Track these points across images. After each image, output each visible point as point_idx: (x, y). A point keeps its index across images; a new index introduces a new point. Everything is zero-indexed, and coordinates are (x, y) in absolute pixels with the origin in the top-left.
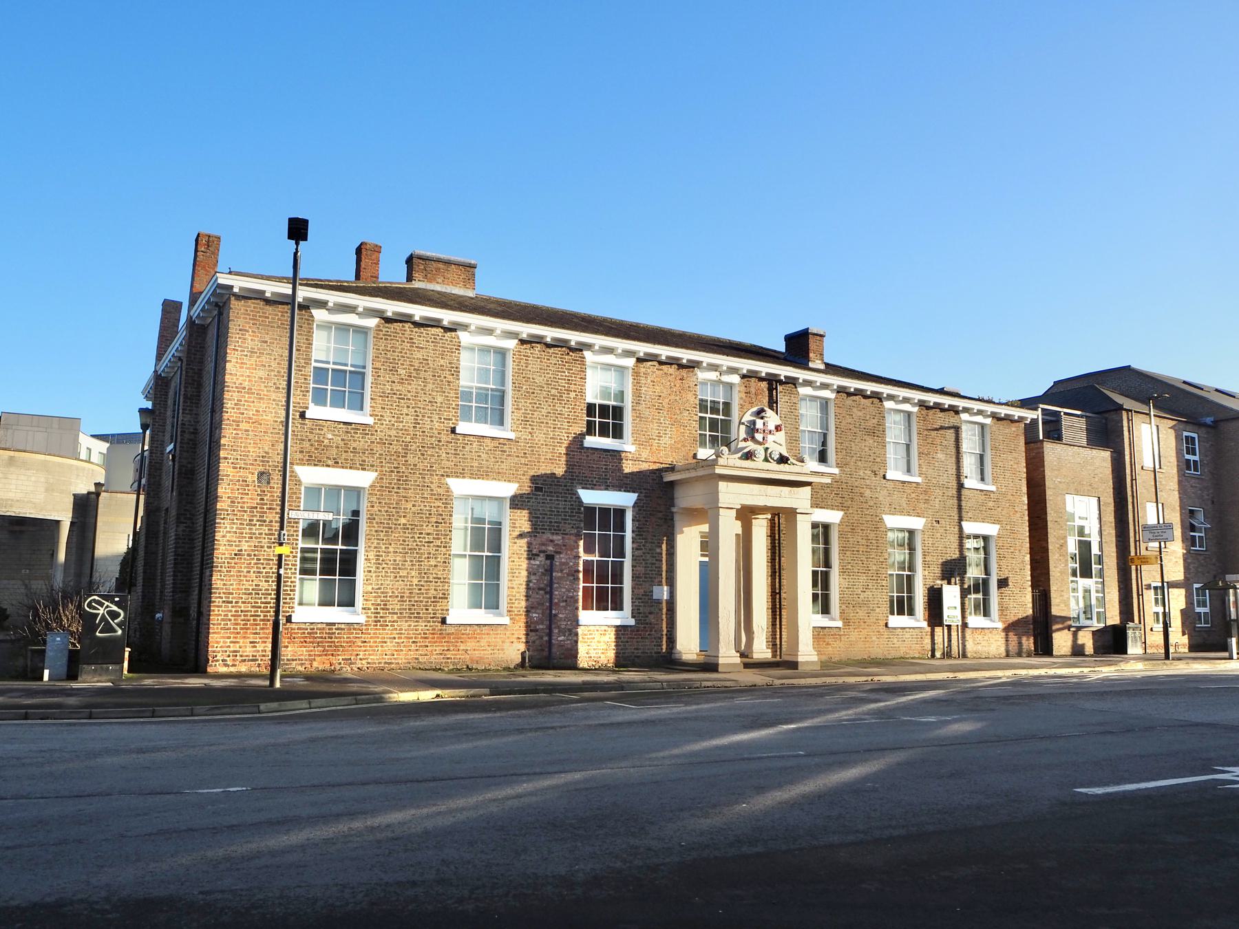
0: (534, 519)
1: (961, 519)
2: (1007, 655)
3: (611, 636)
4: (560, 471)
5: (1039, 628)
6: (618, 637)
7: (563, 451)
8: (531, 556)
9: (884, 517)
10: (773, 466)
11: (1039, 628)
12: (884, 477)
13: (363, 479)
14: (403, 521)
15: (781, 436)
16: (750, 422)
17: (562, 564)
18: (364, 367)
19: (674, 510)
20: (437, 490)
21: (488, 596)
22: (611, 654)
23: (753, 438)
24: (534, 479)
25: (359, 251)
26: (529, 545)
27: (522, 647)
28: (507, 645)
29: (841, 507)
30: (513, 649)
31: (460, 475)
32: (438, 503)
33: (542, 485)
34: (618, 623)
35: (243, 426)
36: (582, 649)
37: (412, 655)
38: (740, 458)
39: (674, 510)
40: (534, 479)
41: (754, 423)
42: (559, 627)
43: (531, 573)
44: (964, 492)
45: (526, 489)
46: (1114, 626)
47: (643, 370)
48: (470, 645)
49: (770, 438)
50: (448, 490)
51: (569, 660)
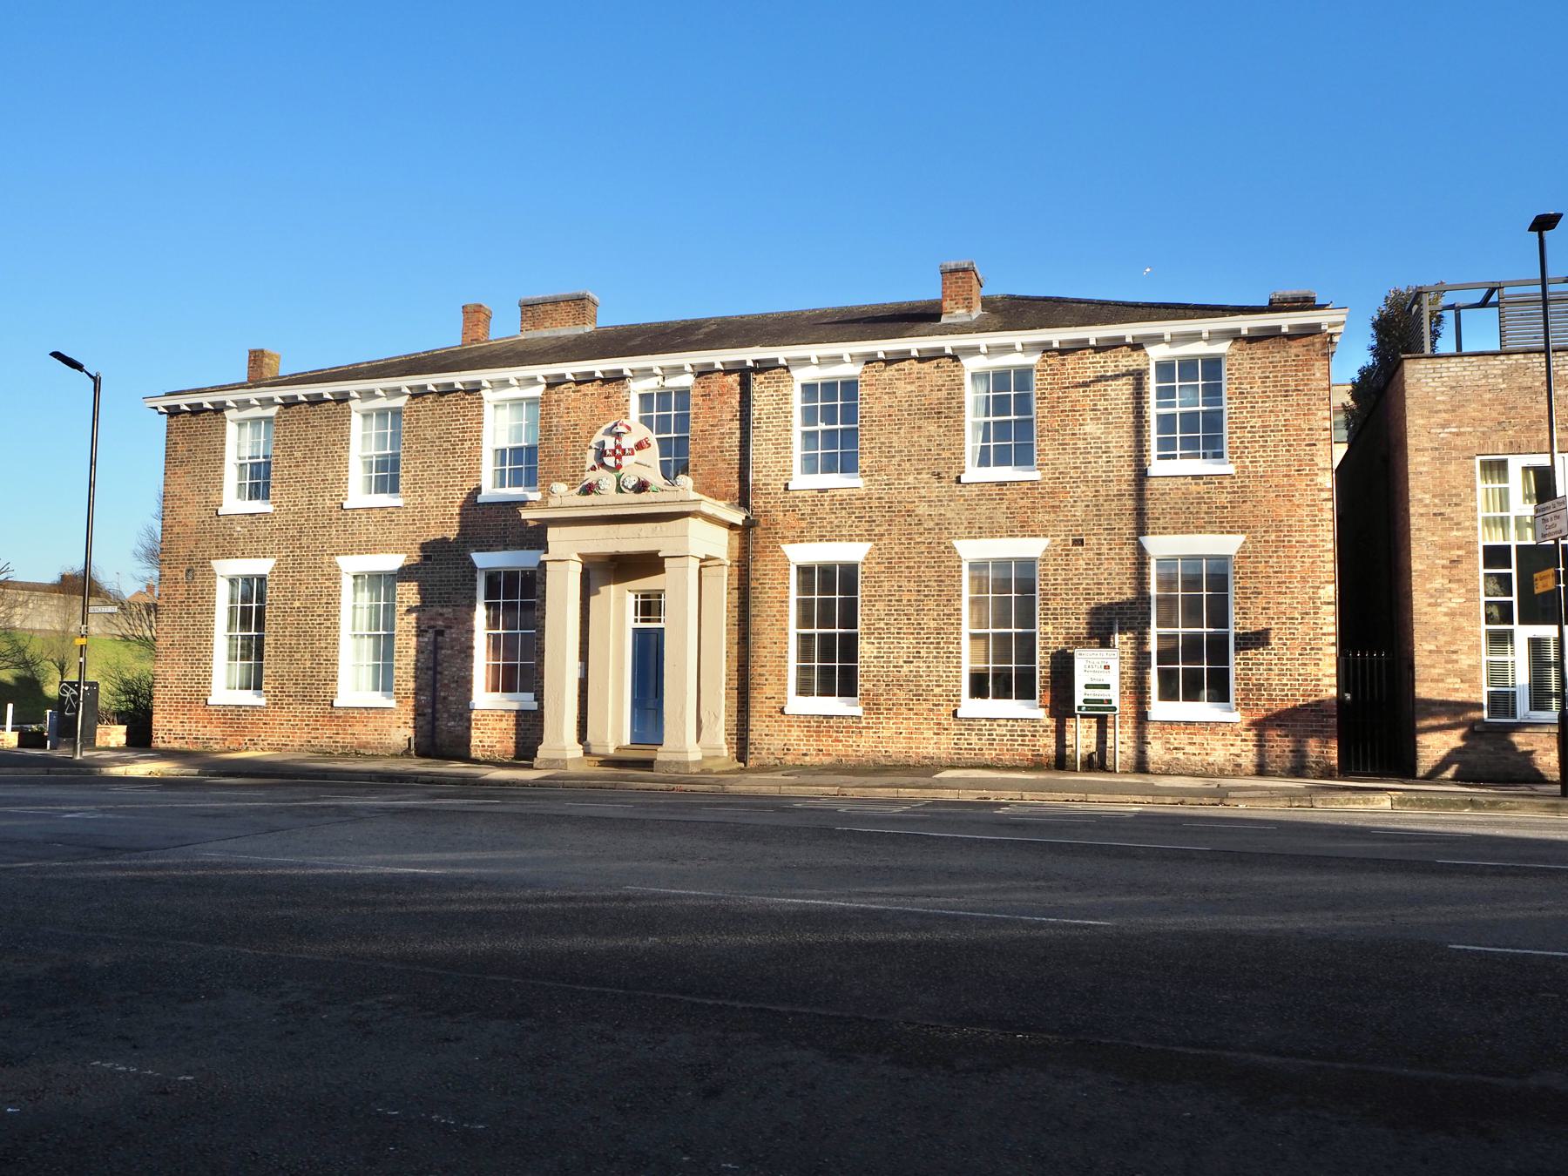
0: (422, 591)
1: (1141, 530)
2: (1261, 770)
3: (509, 723)
4: (452, 533)
5: (1374, 715)
6: (517, 724)
7: (457, 510)
8: (420, 633)
9: (955, 543)
10: (631, 497)
11: (1374, 715)
12: (958, 480)
14: (297, 604)
17: (453, 640)
20: (327, 570)
21: (384, 679)
22: (511, 744)
23: (603, 465)
24: (423, 547)
25: (582, 298)
26: (418, 619)
27: (410, 733)
28: (394, 730)
29: (869, 536)
30: (401, 732)
31: (349, 551)
32: (328, 584)
33: (433, 552)
34: (515, 706)
35: (176, 530)
36: (476, 737)
37: (305, 737)
40: (423, 547)
41: (603, 443)
42: (448, 712)
43: (419, 651)
44: (1152, 484)
45: (416, 557)
46: (128, 734)
47: (555, 397)
48: (358, 729)
50: (337, 569)
51: (459, 749)
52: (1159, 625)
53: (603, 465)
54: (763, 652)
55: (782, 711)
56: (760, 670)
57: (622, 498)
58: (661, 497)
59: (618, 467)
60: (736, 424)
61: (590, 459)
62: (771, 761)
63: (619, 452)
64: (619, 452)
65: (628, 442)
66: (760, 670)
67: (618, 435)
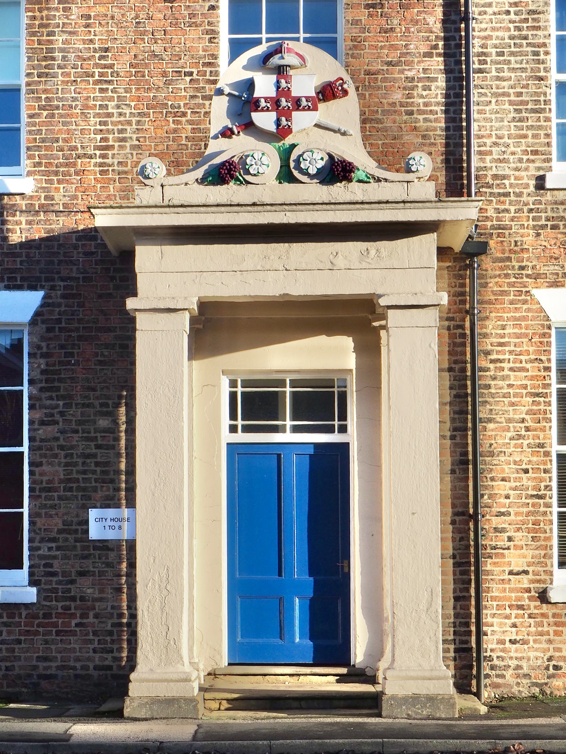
9: (40, 294)
13: (124, 663)
15: (345, 112)
16: (236, 85)
18: (345, 387)
19: (131, 303)
23: (249, 126)
38: (203, 181)
39: (131, 303)
41: (250, 85)
49: (301, 120)
52: (22, 453)
53: (249, 126)
54: (501, 488)
55: (543, 597)
56: (496, 522)
57: (290, 192)
58: (374, 192)
59: (283, 132)
60: (437, 63)
61: (219, 113)
62: (523, 690)
63: (285, 104)
64: (285, 104)
65: (303, 85)
66: (496, 522)
67: (281, 71)
